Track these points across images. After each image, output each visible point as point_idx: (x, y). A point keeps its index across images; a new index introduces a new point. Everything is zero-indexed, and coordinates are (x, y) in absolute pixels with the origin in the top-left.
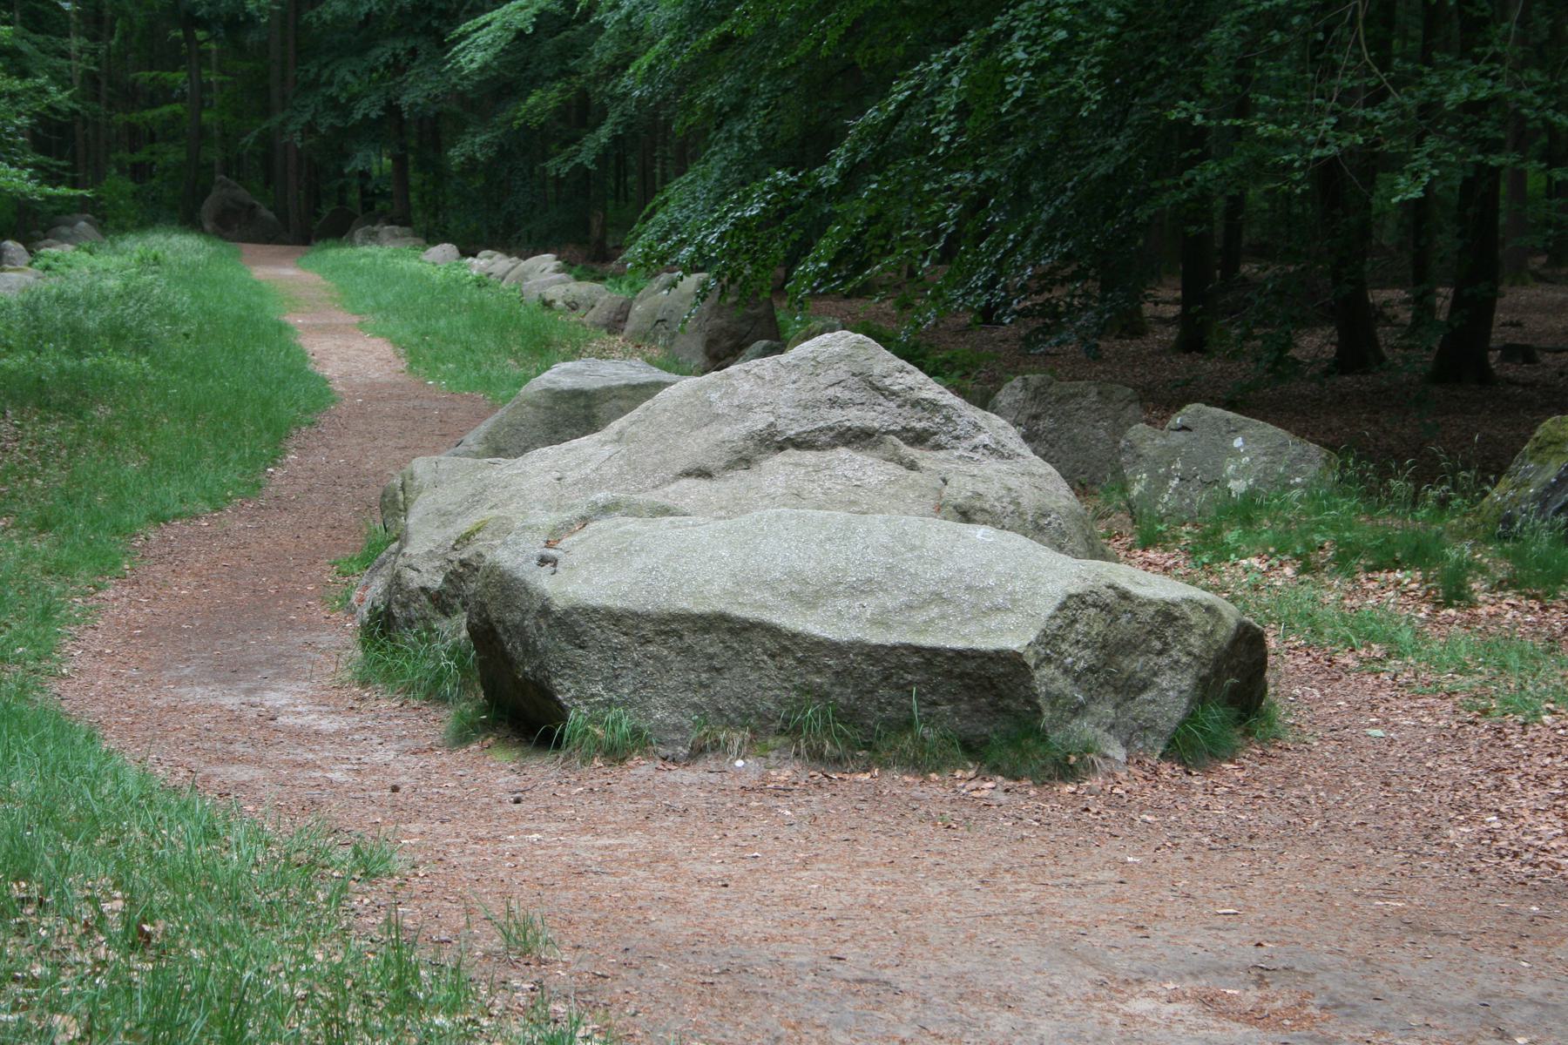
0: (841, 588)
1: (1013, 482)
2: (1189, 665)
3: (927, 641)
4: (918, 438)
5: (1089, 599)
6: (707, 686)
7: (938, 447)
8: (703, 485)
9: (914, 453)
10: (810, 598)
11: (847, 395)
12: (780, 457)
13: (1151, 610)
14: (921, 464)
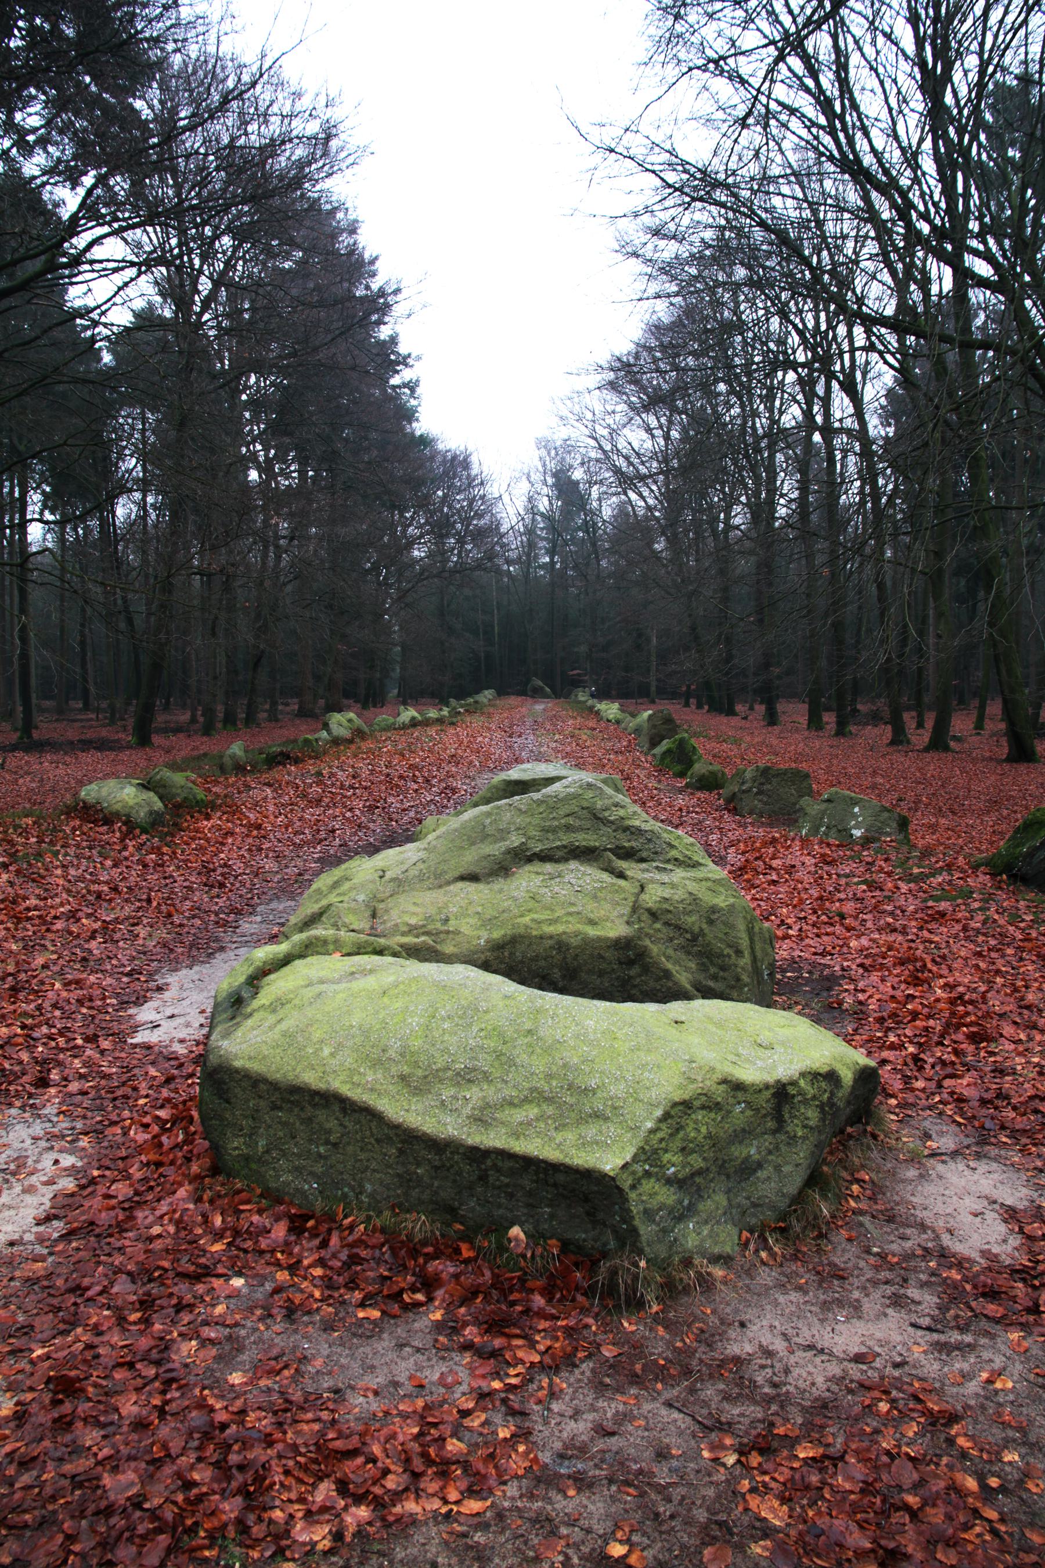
0: (450, 1073)
1: (692, 886)
2: (804, 1138)
3: (521, 1147)
4: (629, 854)
5: (697, 1103)
6: (326, 1158)
7: (642, 860)
8: (471, 887)
9: (622, 864)
10: (418, 1082)
11: (578, 823)
12: (528, 868)
13: (768, 1094)
14: (628, 873)
